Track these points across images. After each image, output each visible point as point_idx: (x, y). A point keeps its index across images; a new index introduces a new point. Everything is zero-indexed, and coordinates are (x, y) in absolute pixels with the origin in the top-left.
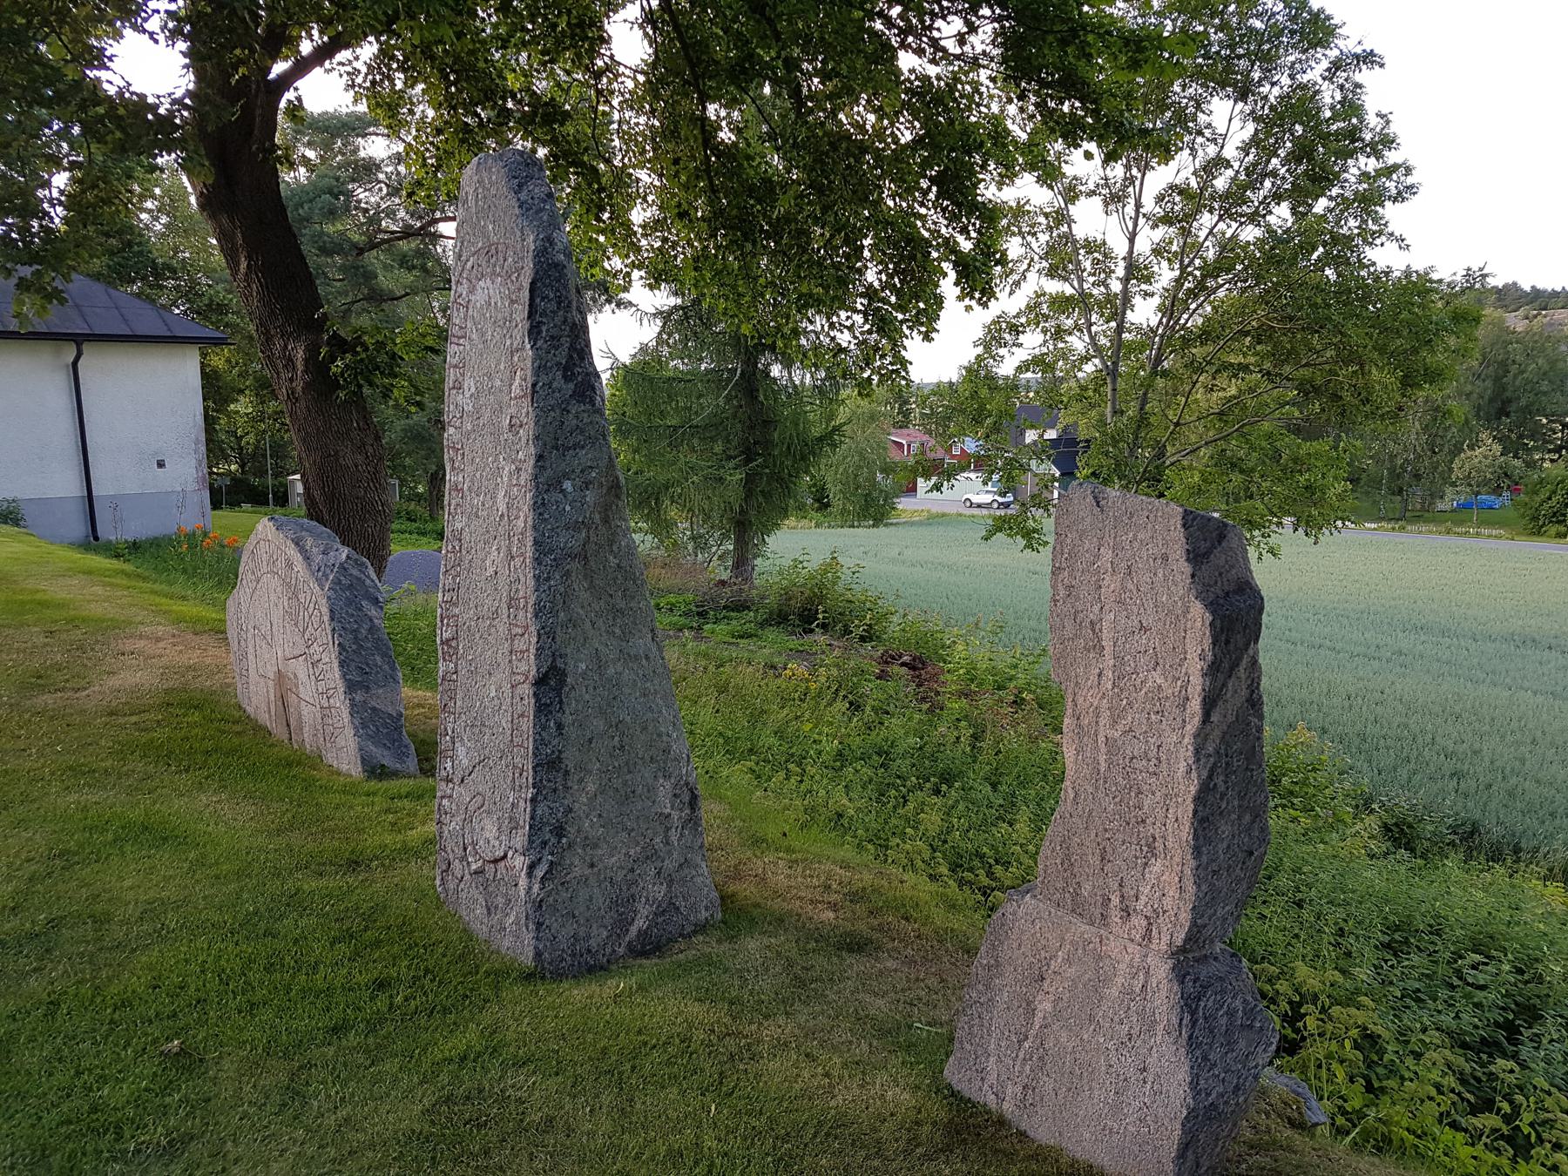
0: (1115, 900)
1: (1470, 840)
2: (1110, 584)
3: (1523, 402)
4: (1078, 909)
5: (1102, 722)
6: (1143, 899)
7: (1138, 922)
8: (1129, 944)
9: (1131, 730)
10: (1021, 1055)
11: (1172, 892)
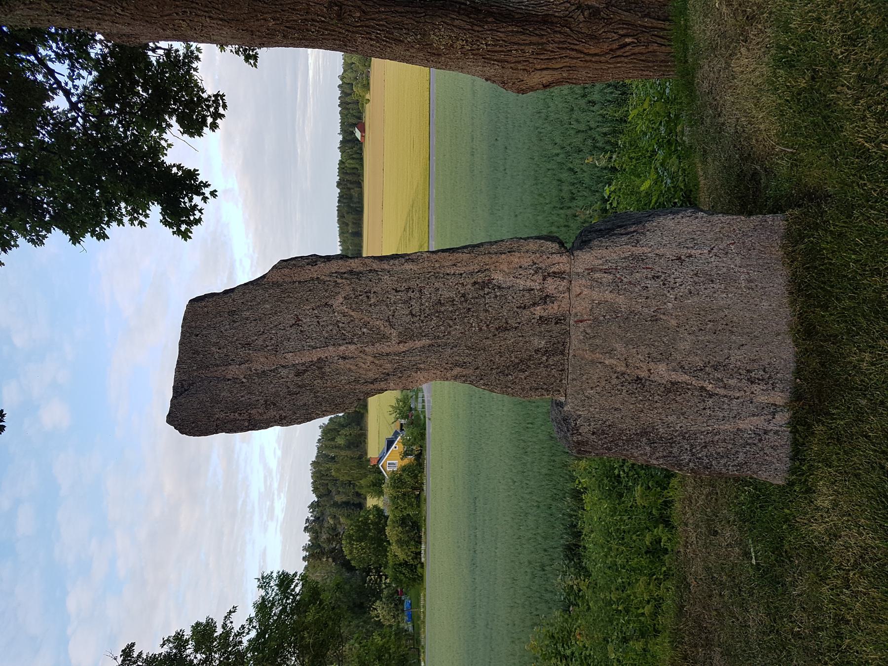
0: (538, 311)
1: (573, 551)
2: (261, 362)
3: (355, 596)
4: (558, 348)
5: (386, 350)
6: (529, 284)
7: (551, 286)
8: (573, 293)
9: (388, 320)
10: (722, 392)
11: (515, 259)
